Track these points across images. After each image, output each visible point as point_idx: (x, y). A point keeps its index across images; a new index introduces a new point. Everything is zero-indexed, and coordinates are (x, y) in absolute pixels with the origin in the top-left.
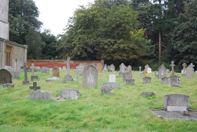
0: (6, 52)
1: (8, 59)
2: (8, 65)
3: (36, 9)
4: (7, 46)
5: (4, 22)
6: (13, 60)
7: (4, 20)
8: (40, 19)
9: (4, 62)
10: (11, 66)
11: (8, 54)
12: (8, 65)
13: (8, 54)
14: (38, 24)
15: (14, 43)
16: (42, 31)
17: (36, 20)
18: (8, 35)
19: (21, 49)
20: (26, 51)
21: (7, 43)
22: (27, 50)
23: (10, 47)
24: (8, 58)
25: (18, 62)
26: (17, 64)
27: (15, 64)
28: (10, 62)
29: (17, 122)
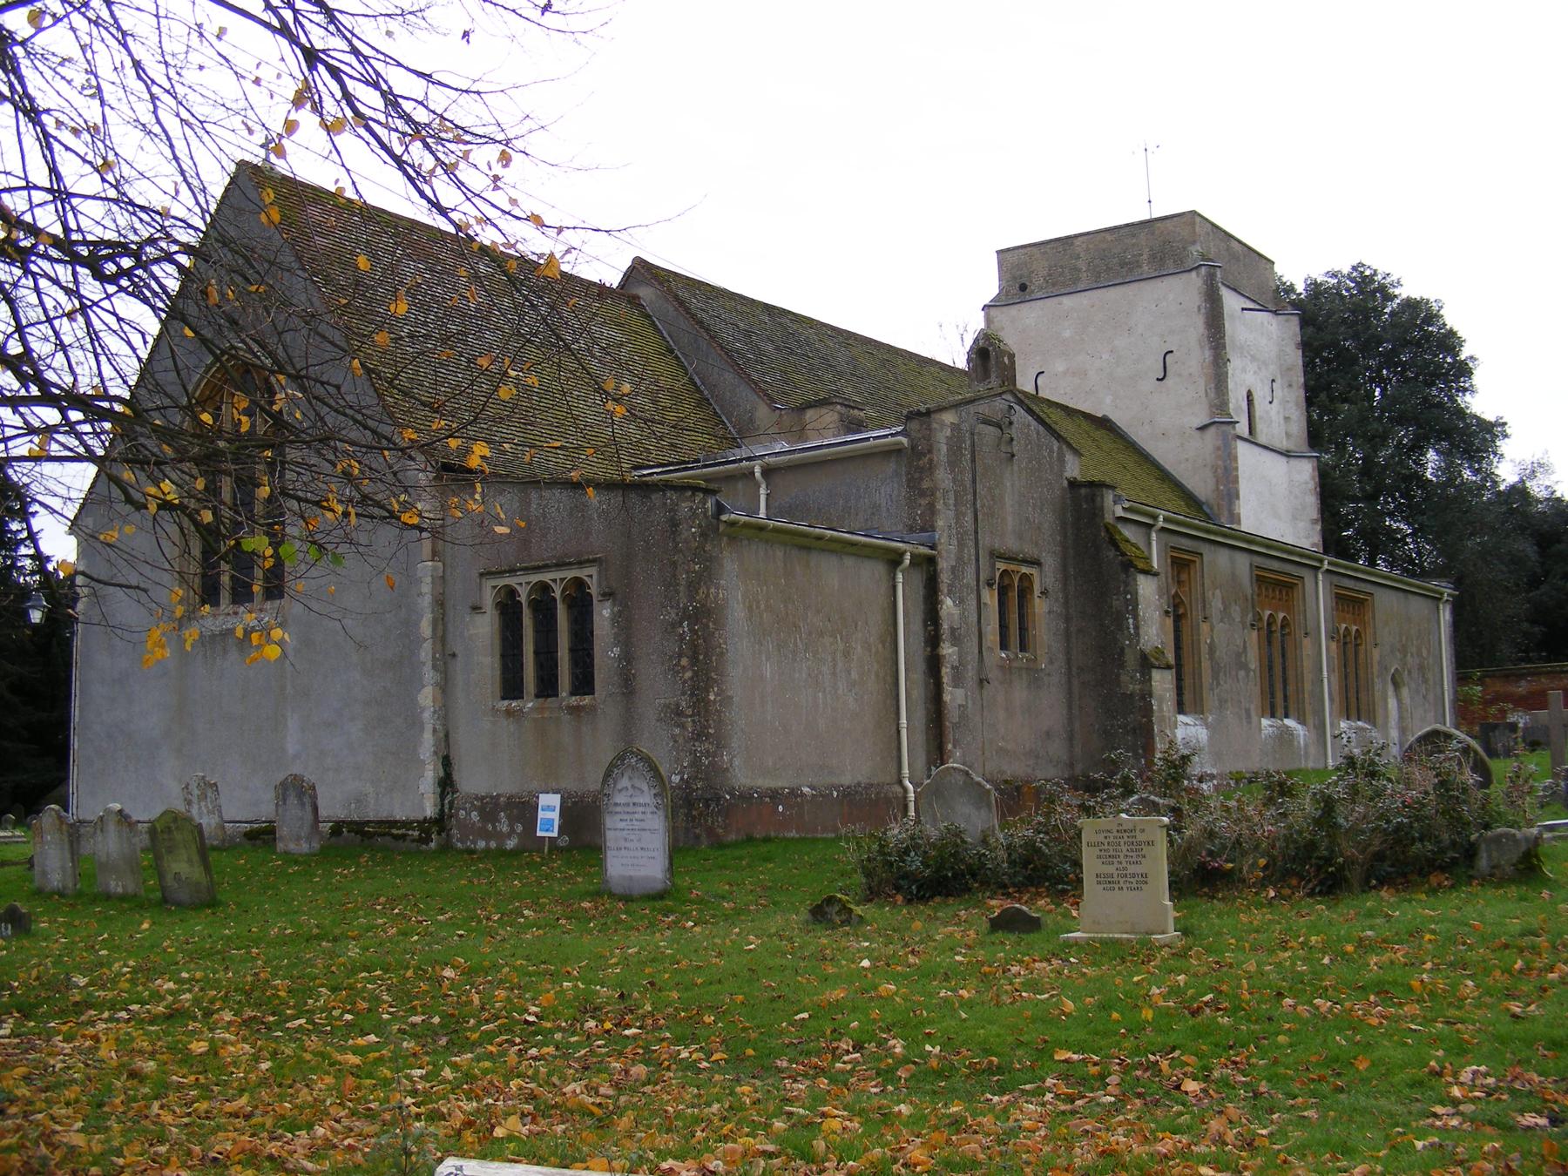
0: (1261, 619)
1: (1278, 660)
2: (1353, 712)
3: (1450, 342)
4: (1260, 580)
5: (1286, 454)
6: (1378, 687)
7: (1284, 444)
8: (1481, 402)
9: (1331, 700)
10: (1372, 720)
11: (1351, 647)
12: (1353, 712)
13: (1351, 647)
14: (1477, 439)
15: (1356, 570)
16: (1507, 473)
17: (1461, 413)
18: (1319, 527)
19: (1418, 607)
20: (1446, 615)
21: (1336, 579)
22: (1448, 608)
23: (1279, 583)
24: (1351, 669)
25: (1405, 692)
26: (1399, 701)
27: (1392, 703)
28: (1363, 696)
29: (598, 1100)
